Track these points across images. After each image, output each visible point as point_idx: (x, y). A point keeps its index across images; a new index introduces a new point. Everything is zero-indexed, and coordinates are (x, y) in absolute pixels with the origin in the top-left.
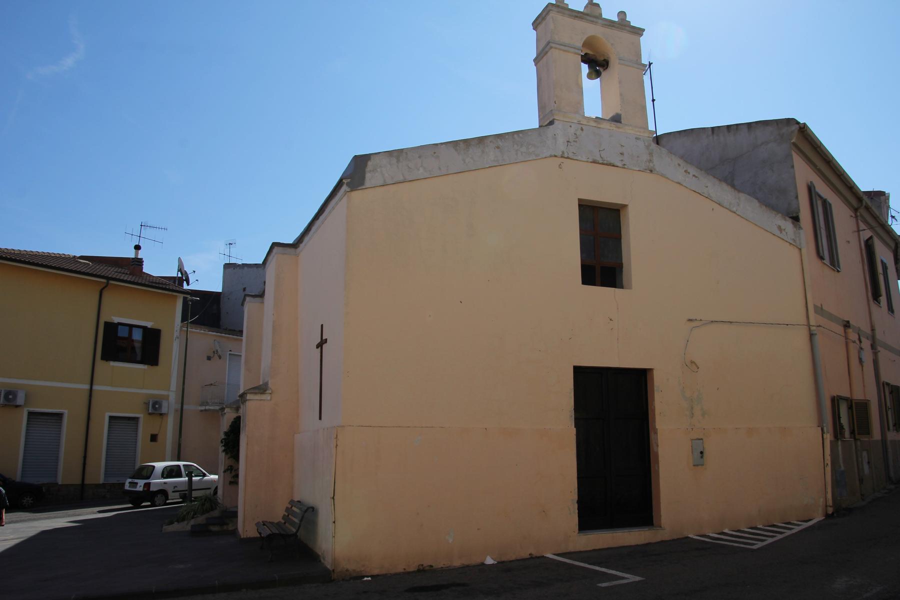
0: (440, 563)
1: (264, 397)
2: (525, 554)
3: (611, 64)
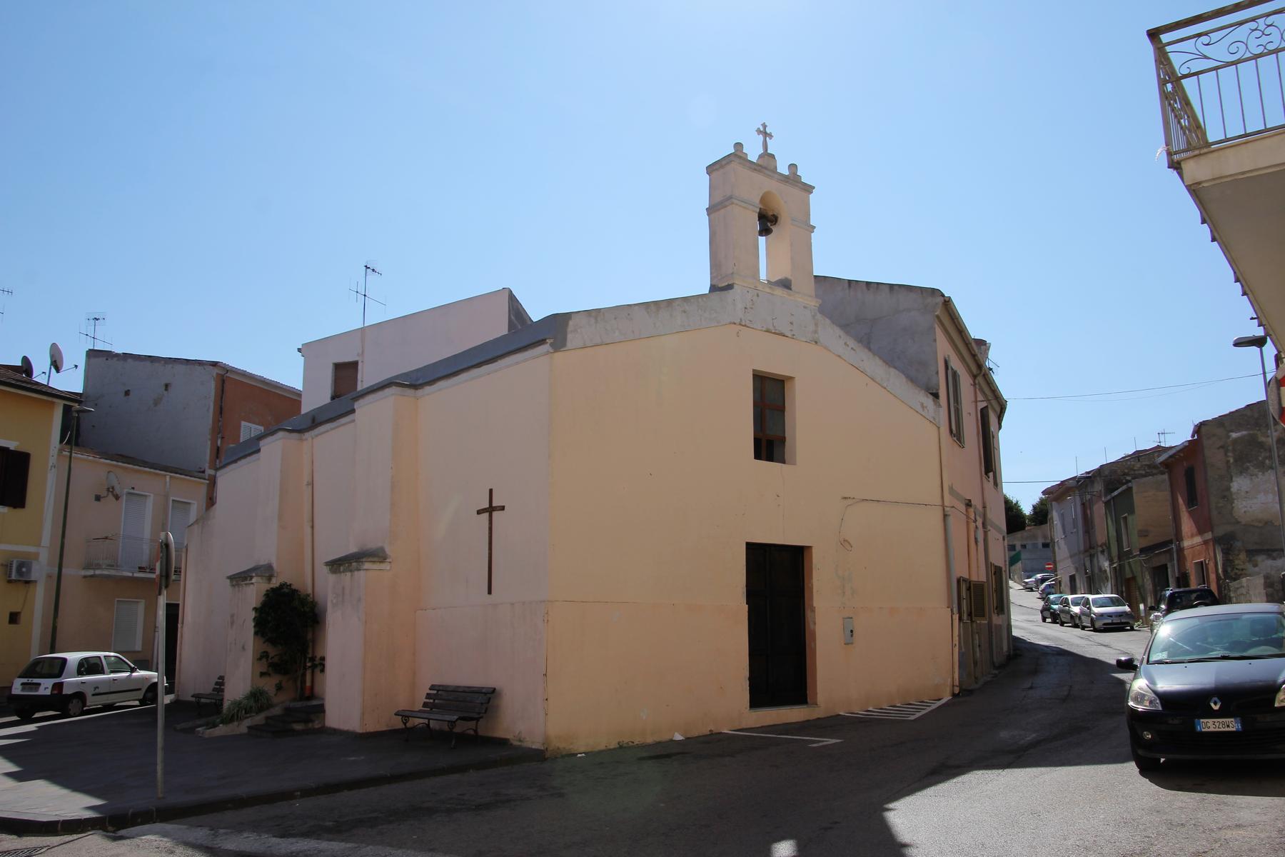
1: (383, 566)
3: (782, 220)
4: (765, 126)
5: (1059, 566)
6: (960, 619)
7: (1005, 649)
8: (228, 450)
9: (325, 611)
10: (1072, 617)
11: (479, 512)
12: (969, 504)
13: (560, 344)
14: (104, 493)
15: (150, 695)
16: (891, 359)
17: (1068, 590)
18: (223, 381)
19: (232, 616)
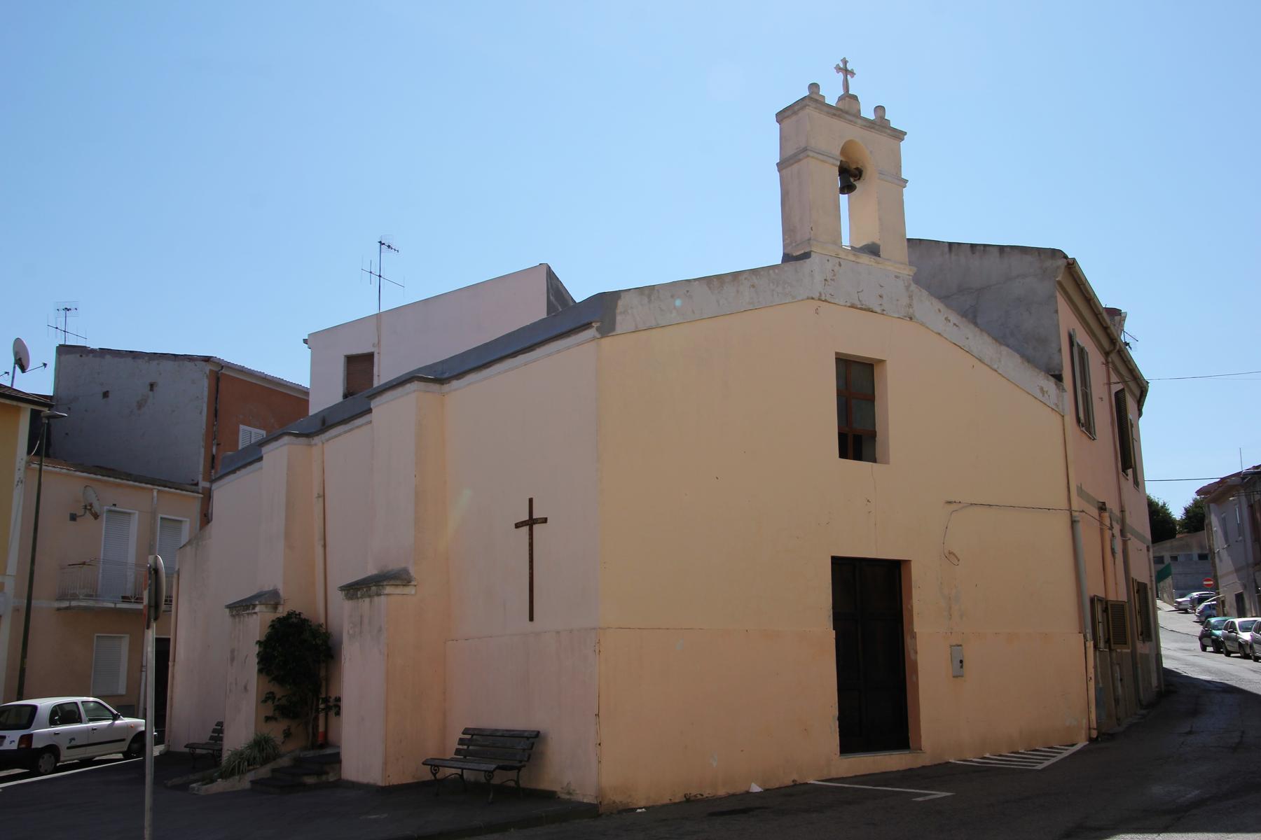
0: (707, 793)
1: (407, 590)
2: (788, 781)
3: (869, 172)
4: (845, 62)
5: (1222, 583)
6: (1096, 647)
7: (1154, 682)
8: (225, 458)
9: (341, 643)
10: (1240, 645)
11: (518, 526)
12: (1102, 508)
13: (607, 329)
14: (80, 512)
15: (135, 746)
16: (1004, 336)
17: (1235, 612)
18: (218, 379)
19: (233, 651)
